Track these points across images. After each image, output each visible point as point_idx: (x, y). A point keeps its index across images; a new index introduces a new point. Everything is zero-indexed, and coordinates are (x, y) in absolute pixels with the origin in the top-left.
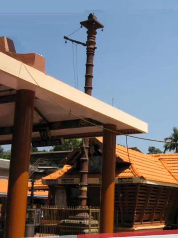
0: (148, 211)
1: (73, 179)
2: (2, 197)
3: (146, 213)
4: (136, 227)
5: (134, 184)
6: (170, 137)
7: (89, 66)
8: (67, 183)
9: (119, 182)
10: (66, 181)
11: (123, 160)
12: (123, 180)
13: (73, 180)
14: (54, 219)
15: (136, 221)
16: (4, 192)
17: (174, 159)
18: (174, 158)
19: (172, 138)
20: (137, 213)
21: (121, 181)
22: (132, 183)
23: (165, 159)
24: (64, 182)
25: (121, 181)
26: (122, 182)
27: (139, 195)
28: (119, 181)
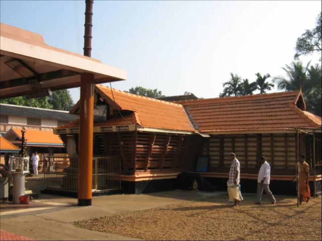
0: (140, 159)
1: (111, 126)
2: (49, 147)
3: (165, 160)
4: (138, 175)
5: (130, 131)
6: (229, 82)
7: (88, 15)
8: (121, 130)
9: (117, 130)
10: (73, 130)
11: (121, 108)
12: (120, 128)
13: (111, 127)
14: (107, 172)
15: (138, 169)
16: (50, 142)
17: (202, 105)
18: (202, 104)
19: (231, 82)
20: (150, 161)
21: (119, 129)
22: (128, 131)
23: (190, 105)
24: (119, 129)
25: (103, 130)
26: (119, 130)
27: (137, 142)
28: (127, 127)
